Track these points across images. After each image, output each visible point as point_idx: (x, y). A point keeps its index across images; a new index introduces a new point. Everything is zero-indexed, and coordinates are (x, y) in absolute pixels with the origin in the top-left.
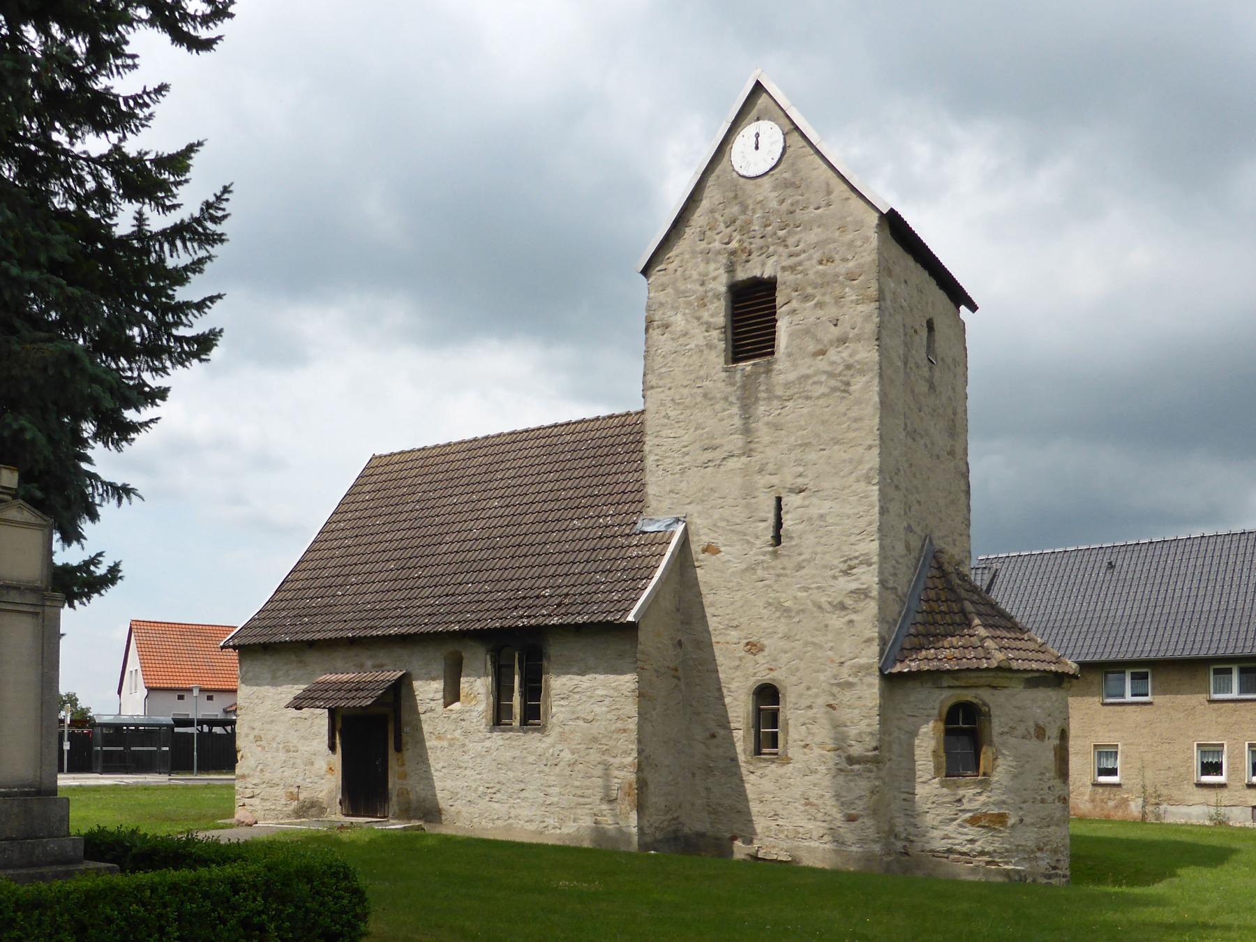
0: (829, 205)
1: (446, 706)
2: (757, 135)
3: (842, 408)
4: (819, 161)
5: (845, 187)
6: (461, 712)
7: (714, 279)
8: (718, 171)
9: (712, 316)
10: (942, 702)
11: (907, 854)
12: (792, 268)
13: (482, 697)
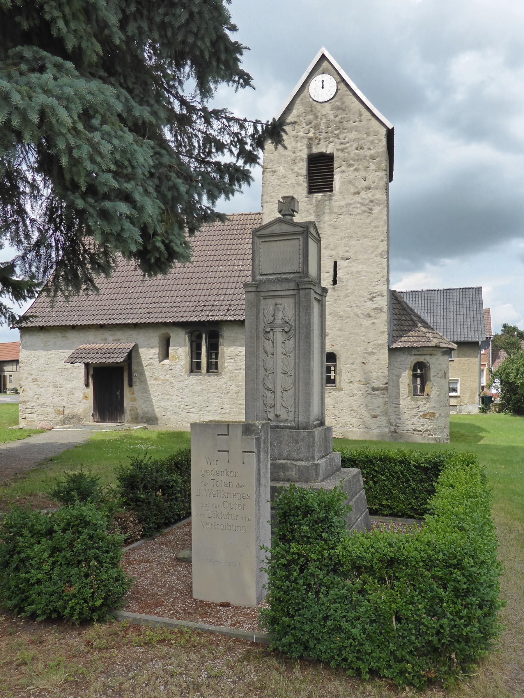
0: (360, 121)
1: (160, 362)
2: (323, 81)
3: (368, 221)
4: (355, 99)
5: (368, 114)
6: (169, 365)
7: (300, 151)
8: (302, 96)
9: (300, 169)
10: (412, 362)
11: (396, 432)
12: (342, 150)
13: (183, 358)
